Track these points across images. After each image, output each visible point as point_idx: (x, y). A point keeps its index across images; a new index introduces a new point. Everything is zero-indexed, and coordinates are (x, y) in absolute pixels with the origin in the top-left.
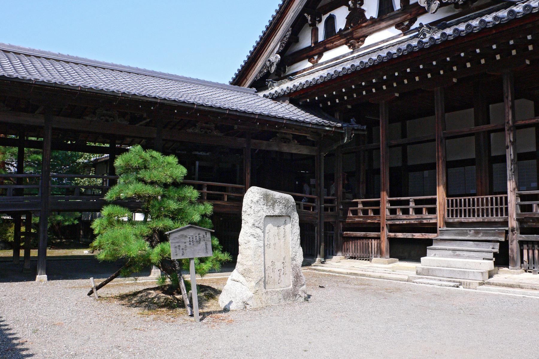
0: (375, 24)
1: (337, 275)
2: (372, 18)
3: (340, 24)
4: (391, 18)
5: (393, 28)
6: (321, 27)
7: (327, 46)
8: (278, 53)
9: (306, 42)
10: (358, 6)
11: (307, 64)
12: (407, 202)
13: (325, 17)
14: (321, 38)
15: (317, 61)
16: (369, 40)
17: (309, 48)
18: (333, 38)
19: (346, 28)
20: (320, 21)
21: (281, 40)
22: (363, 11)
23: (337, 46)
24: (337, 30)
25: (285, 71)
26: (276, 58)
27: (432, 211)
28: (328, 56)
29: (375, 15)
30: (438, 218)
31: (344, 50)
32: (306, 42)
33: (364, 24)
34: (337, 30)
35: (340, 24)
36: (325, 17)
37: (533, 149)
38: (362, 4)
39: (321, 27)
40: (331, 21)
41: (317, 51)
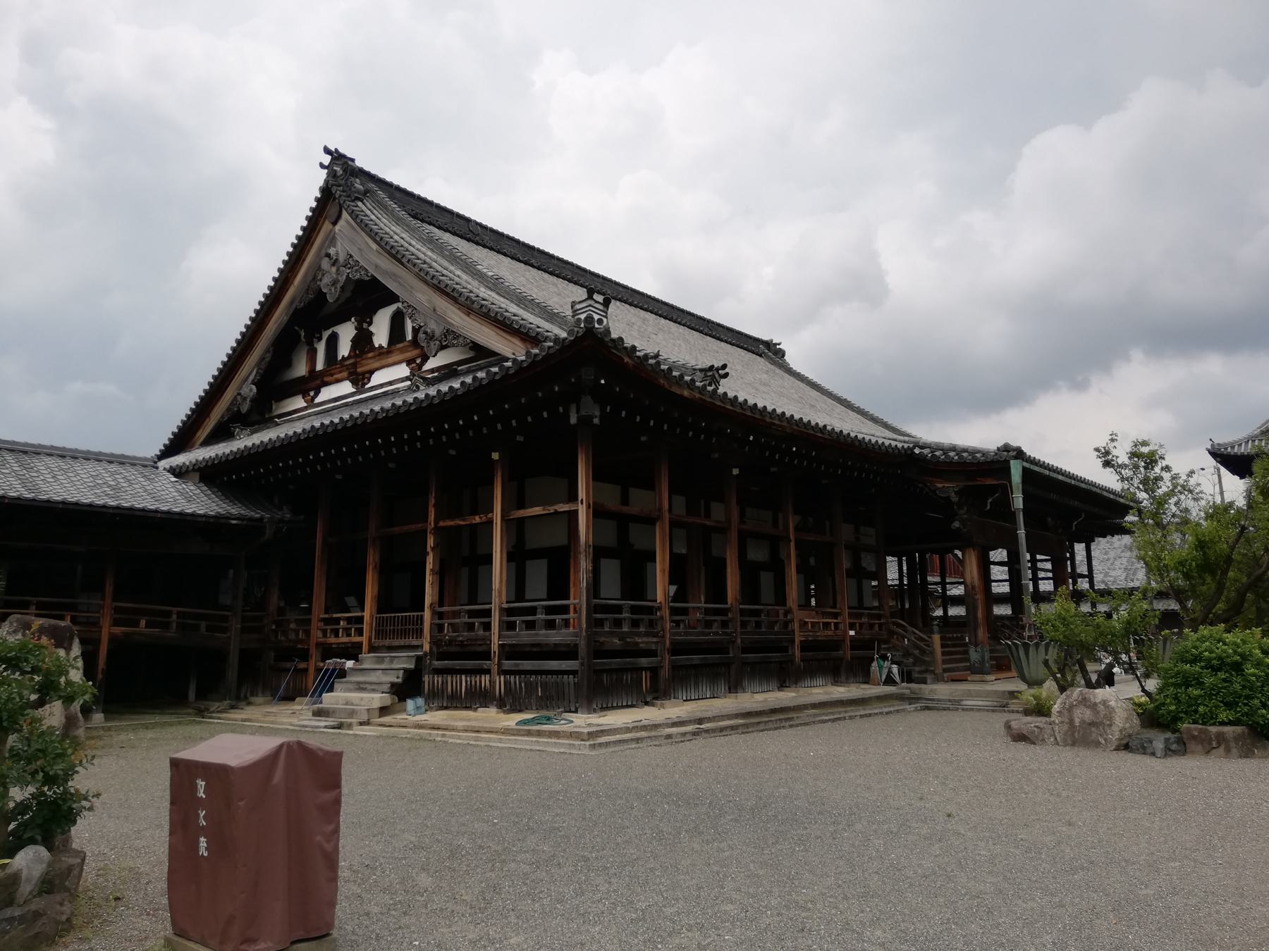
0: (385, 356)
1: (643, 734)
2: (381, 347)
3: (344, 350)
4: (402, 351)
5: (404, 365)
6: (321, 348)
7: (326, 379)
8: (253, 383)
9: (301, 370)
10: (365, 325)
11: (299, 402)
12: (169, 614)
13: (326, 334)
14: (320, 366)
15: (313, 399)
16: (378, 378)
17: (301, 379)
18: (334, 369)
19: (349, 357)
20: (320, 339)
21: (258, 364)
22: (371, 334)
23: (338, 381)
24: (340, 358)
25: (270, 410)
26: (250, 390)
27: (360, 632)
28: (327, 393)
29: (385, 344)
30: (364, 639)
31: (346, 388)
32: (301, 370)
33: (370, 355)
34: (340, 358)
35: (344, 350)
36: (326, 334)
37: (1083, 545)
38: (370, 323)
39: (321, 348)
40: (333, 342)
41: (313, 384)
